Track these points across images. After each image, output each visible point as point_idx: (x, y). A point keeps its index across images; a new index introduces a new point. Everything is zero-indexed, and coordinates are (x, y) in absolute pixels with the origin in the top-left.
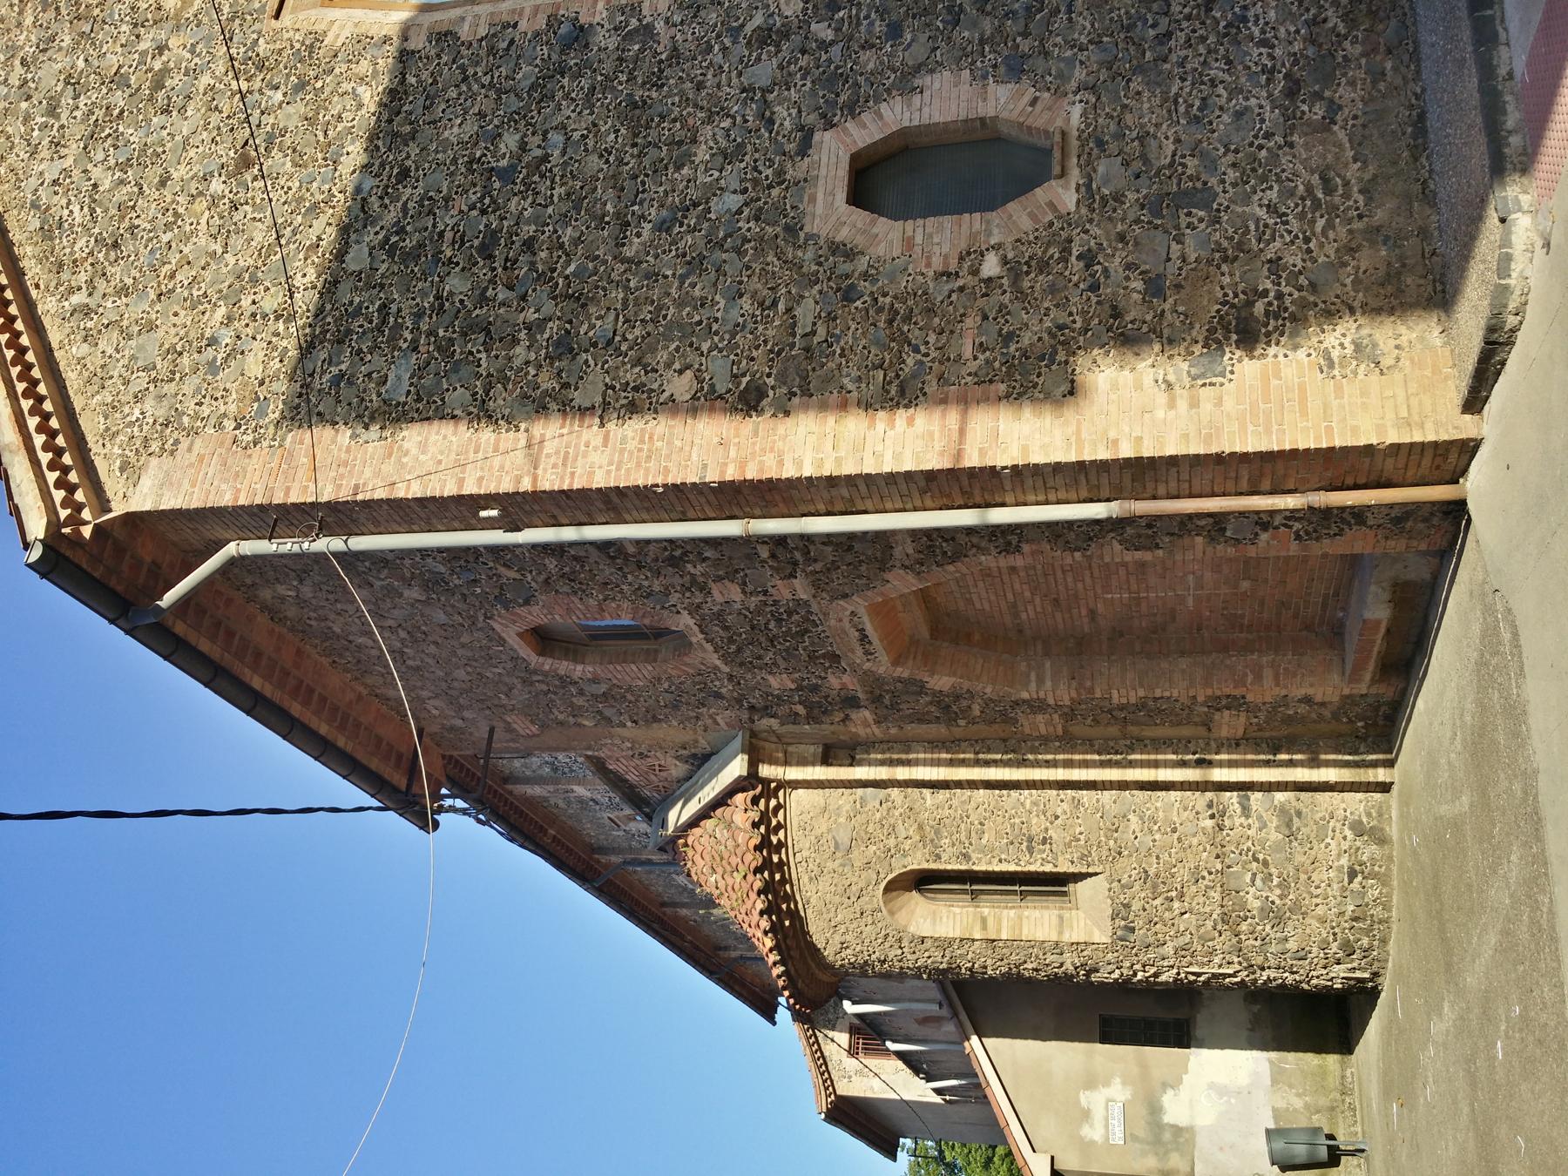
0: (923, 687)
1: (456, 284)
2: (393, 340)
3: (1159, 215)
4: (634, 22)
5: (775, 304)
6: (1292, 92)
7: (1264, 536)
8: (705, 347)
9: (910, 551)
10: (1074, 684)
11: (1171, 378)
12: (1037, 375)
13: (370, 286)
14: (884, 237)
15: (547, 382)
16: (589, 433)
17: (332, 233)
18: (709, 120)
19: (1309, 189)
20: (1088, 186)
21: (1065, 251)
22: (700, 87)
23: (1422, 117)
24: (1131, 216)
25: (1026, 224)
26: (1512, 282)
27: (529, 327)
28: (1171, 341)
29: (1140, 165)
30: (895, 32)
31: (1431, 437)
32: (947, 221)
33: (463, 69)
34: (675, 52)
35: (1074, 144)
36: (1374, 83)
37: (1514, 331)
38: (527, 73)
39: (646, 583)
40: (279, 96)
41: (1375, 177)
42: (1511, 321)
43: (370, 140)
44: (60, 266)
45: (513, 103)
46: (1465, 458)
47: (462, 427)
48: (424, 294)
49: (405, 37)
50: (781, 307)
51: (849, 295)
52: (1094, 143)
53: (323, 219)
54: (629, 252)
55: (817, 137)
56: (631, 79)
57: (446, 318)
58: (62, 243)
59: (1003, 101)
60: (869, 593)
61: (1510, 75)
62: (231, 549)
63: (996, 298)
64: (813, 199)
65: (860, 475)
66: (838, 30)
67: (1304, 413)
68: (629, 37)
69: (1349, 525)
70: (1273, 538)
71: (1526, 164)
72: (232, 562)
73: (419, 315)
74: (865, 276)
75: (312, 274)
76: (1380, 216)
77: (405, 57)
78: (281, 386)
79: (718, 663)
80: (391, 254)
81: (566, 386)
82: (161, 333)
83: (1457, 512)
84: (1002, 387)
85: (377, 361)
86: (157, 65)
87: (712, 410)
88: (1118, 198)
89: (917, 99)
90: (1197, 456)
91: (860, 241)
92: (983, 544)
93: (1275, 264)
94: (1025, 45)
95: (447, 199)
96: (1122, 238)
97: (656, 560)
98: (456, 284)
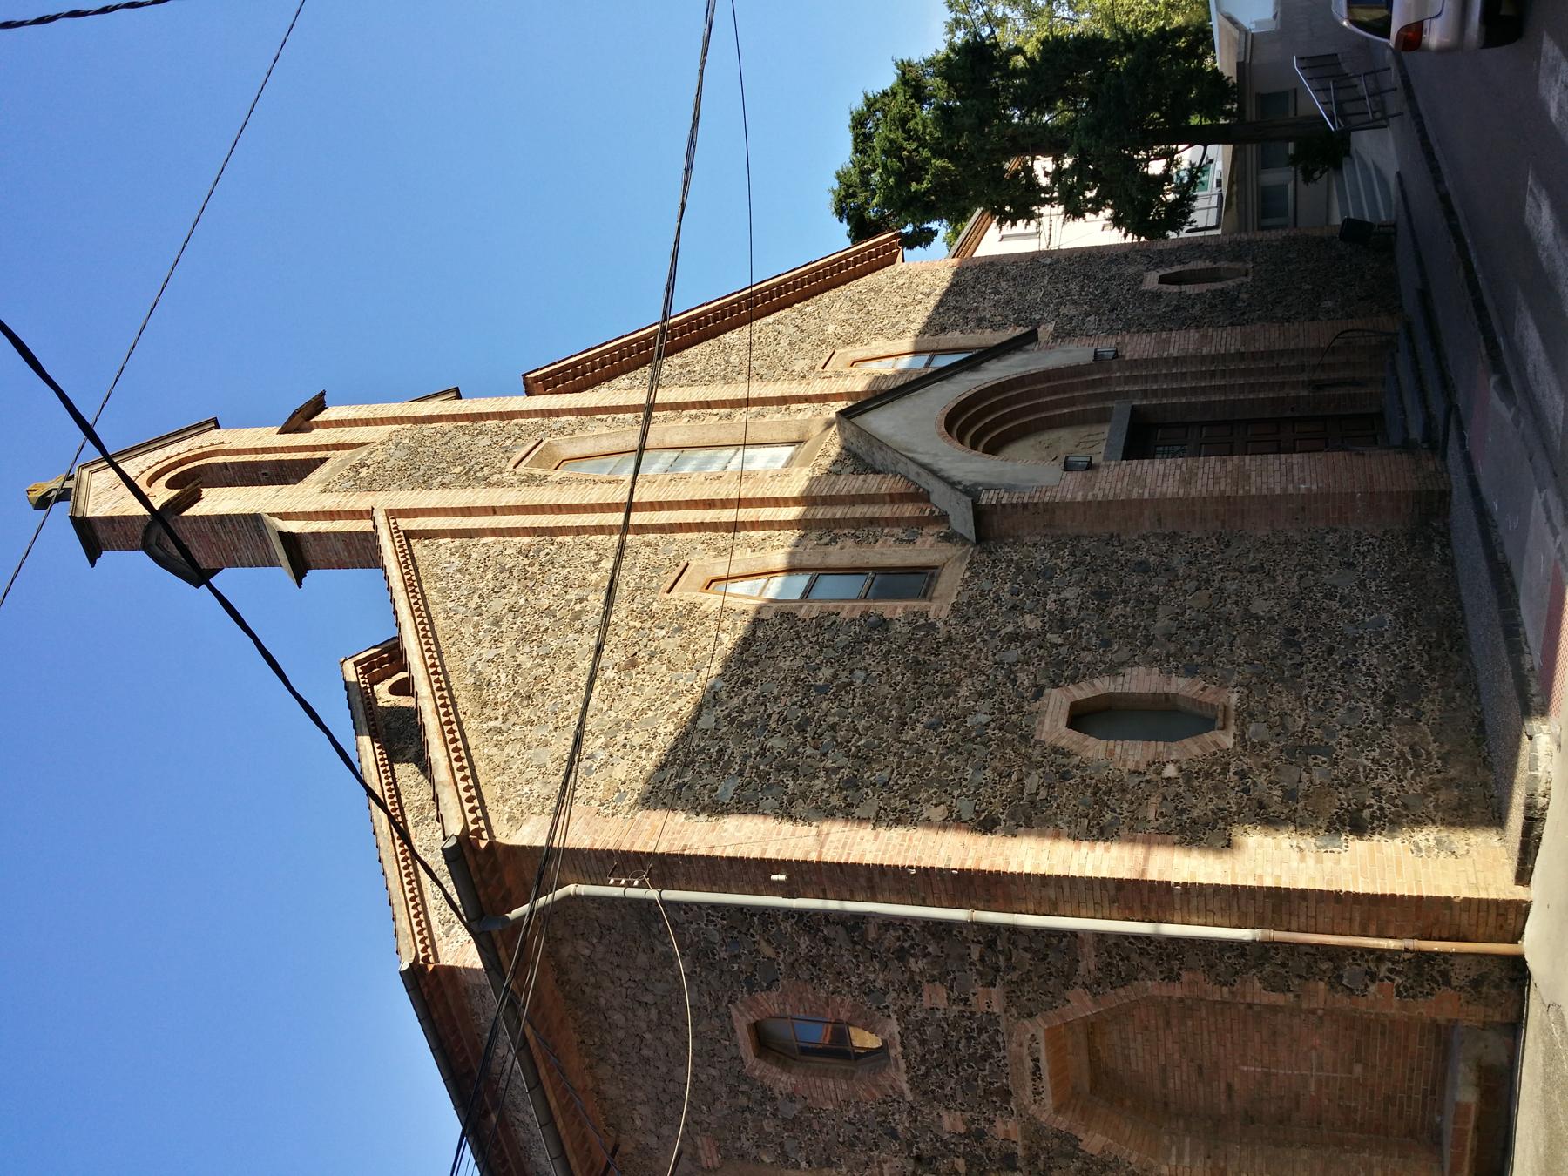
0: (1075, 1147)
1: (776, 742)
2: (725, 770)
3: (1293, 756)
4: (922, 621)
5: (1010, 775)
6: (1390, 700)
7: (1373, 988)
8: (956, 793)
9: (1092, 968)
10: (1209, 1163)
11: (1302, 845)
12: (1206, 830)
13: (712, 738)
14: (1093, 748)
15: (836, 800)
16: (866, 832)
17: (691, 707)
18: (971, 675)
19: (1402, 754)
20: (1243, 736)
21: (1225, 771)
22: (965, 658)
23: (1482, 723)
24: (1273, 755)
25: (1196, 751)
26: (1539, 774)
27: (827, 770)
28: (1302, 825)
29: (1280, 727)
30: (1106, 644)
31: (1493, 896)
32: (1140, 744)
33: (798, 633)
34: (949, 639)
35: (1233, 713)
36: (1448, 703)
37: (1544, 809)
38: (842, 639)
39: (872, 977)
40: (663, 632)
41: (1449, 752)
42: (1542, 801)
43: (726, 661)
44: (485, 705)
45: (832, 653)
46: (1521, 919)
47: (770, 820)
48: (752, 746)
49: (758, 612)
50: (1014, 777)
51: (1064, 776)
52: (1245, 716)
53: (684, 700)
54: (904, 737)
55: (1047, 691)
56: (917, 649)
57: (766, 761)
58: (488, 694)
59: (1180, 685)
60: (1050, 1013)
61: (1532, 669)
62: (571, 889)
63: (1173, 789)
64: (1041, 723)
65: (1066, 877)
66: (1066, 639)
67: (1400, 873)
68: (919, 628)
69: (1437, 982)
70: (1380, 991)
71: (1544, 711)
72: (568, 897)
73: (748, 756)
74: (1078, 767)
75: (671, 727)
76: (1453, 773)
77: (756, 622)
78: (639, 786)
79: (905, 1086)
80: (731, 723)
81: (851, 805)
82: (553, 748)
83: (1517, 972)
84: (1177, 838)
85: (711, 779)
86: (578, 608)
87: (958, 828)
88: (1264, 745)
89: (1120, 679)
90: (1321, 891)
91: (1075, 748)
92: (1151, 968)
93: (1378, 793)
94: (1198, 660)
95: (776, 698)
96: (1266, 766)
97: (888, 950)
98: (776, 742)
